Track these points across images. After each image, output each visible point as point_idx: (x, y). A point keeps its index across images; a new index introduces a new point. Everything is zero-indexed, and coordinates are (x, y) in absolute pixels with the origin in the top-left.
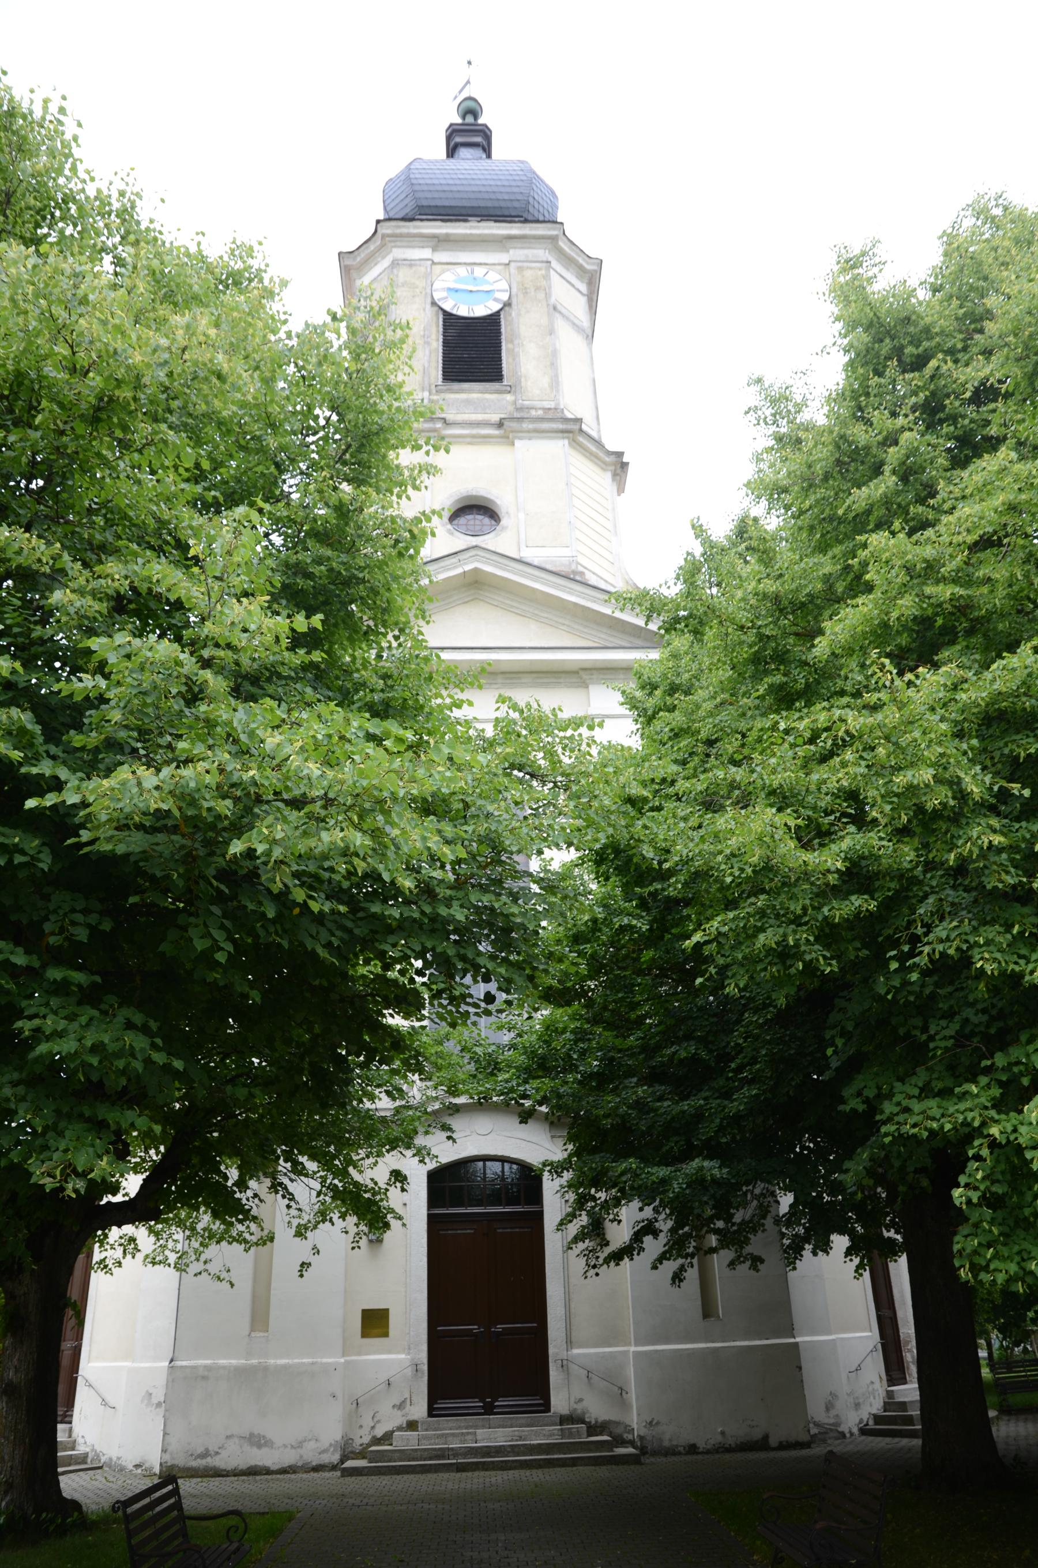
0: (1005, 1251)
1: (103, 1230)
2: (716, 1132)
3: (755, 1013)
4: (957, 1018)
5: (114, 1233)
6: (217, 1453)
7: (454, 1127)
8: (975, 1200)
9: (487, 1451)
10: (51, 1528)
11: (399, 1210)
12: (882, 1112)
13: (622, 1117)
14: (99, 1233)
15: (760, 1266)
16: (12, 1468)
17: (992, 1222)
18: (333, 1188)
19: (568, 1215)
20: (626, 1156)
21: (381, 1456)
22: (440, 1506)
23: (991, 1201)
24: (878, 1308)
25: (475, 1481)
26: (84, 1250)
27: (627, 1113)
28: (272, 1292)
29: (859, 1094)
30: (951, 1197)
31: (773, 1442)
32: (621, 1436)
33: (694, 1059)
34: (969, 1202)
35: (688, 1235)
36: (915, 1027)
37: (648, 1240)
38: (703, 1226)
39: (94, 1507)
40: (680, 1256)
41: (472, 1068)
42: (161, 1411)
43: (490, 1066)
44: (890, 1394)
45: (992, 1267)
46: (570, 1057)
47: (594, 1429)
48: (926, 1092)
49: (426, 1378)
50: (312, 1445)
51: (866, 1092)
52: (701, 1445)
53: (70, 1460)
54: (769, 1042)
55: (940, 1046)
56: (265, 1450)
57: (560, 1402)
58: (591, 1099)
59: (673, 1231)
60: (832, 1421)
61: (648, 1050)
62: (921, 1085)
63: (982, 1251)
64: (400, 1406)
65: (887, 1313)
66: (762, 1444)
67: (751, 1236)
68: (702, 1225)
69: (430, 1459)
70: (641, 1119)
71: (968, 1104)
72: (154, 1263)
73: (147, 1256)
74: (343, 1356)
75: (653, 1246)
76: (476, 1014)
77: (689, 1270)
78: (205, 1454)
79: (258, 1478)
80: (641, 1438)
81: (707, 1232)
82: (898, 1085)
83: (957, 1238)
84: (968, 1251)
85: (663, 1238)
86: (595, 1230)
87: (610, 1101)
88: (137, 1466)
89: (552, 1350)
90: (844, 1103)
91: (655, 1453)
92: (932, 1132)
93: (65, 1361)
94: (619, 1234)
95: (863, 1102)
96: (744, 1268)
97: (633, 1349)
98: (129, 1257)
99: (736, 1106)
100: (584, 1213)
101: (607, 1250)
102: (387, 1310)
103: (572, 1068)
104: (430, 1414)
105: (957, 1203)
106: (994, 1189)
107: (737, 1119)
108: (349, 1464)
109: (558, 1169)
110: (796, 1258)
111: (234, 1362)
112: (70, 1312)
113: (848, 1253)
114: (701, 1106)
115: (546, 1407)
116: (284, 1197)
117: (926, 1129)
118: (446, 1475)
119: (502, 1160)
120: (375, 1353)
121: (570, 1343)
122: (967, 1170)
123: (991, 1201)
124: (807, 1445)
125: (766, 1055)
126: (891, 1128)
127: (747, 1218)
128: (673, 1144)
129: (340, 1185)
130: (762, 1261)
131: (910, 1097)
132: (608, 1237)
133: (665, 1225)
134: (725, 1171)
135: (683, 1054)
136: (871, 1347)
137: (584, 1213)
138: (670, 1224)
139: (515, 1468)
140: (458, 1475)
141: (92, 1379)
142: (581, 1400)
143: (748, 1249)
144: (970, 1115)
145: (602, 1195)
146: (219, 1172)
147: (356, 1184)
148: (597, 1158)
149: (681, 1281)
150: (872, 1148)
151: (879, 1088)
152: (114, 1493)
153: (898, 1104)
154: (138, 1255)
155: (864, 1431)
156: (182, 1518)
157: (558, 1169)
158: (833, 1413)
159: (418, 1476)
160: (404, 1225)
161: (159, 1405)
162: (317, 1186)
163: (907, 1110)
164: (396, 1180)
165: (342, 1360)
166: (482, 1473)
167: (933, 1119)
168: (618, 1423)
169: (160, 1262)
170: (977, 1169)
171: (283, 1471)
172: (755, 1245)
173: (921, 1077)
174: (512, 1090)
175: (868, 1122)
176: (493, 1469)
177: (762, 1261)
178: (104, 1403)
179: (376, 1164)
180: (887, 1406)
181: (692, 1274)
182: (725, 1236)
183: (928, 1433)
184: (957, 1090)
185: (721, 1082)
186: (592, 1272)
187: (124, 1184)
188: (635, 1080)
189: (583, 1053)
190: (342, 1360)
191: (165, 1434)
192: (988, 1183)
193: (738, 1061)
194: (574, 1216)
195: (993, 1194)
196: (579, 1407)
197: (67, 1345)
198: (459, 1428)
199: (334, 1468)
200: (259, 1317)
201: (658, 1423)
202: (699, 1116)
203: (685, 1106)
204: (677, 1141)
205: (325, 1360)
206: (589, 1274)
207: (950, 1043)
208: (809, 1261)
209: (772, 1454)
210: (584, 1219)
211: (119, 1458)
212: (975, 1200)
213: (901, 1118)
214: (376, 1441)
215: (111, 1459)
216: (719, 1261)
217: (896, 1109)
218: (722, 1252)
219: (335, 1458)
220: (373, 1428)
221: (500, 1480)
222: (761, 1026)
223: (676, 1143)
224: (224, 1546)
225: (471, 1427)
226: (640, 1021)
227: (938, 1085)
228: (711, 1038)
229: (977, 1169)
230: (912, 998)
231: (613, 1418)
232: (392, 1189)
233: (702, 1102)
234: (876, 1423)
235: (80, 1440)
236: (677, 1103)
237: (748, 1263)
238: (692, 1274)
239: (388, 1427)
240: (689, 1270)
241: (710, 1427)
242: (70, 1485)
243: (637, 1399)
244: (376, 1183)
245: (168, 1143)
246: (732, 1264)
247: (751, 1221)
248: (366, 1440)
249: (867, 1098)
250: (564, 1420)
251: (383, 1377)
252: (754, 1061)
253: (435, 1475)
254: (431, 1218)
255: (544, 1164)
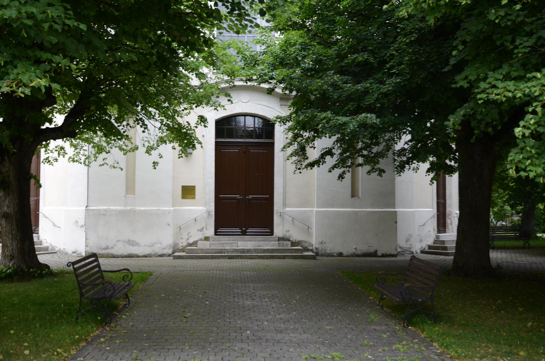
0: (537, 162)
1: (46, 141)
2: (375, 101)
3: (404, 37)
4: (535, 36)
5: (53, 144)
6: (112, 248)
7: (232, 95)
8: (527, 134)
9: (243, 251)
10: (36, 275)
11: (201, 139)
12: (478, 87)
13: (324, 90)
14: (44, 143)
15: (383, 174)
16: (12, 250)
17: (532, 147)
18: (167, 125)
19: (288, 143)
20: (325, 111)
21: (192, 251)
22: (222, 272)
23: (536, 136)
24: (438, 198)
25: (237, 263)
26: (36, 152)
27: (327, 89)
28: (136, 176)
29: (466, 78)
30: (513, 131)
31: (379, 253)
32: (307, 247)
33: (366, 63)
34: (524, 135)
35: (348, 157)
36: (506, 41)
37: (328, 158)
38: (356, 153)
39: (56, 268)
40: (343, 167)
41: (242, 64)
42: (83, 229)
43: (252, 62)
44: (437, 237)
45: (528, 169)
46: (297, 59)
47: (293, 244)
48: (507, 77)
49: (214, 218)
50: (159, 245)
51: (470, 78)
52: (345, 253)
53: (40, 249)
54: (410, 53)
55: (520, 52)
56: (136, 247)
57: (278, 231)
58: (308, 81)
59: (341, 154)
60: (408, 246)
61: (341, 57)
62: (504, 73)
63: (524, 161)
64: (201, 230)
65: (441, 201)
66: (374, 254)
67: (380, 160)
68: (358, 151)
69: (216, 253)
70: (334, 93)
71: (534, 83)
72: (74, 161)
73: (70, 158)
74: (173, 207)
75: (330, 161)
76: (251, 26)
77: (347, 173)
78: (107, 248)
79: (133, 259)
80: (317, 249)
81: (358, 156)
82: (490, 74)
83: (511, 154)
84: (516, 161)
85: (336, 158)
86: (301, 152)
87: (318, 82)
88: (74, 252)
89: (276, 208)
90: (456, 83)
91: (322, 255)
92: (508, 99)
93: (32, 207)
94: (313, 154)
95: (468, 83)
96: (374, 175)
97: (315, 209)
98: (61, 157)
99: (385, 89)
100: (296, 143)
101: (307, 162)
102: (194, 186)
103: (298, 65)
104: (216, 234)
105: (517, 135)
106: (538, 129)
107: (386, 95)
108: (176, 254)
109: (283, 120)
110: (401, 171)
111: (118, 208)
112: (32, 181)
113: (428, 171)
114: (368, 88)
115: (272, 233)
116: (141, 127)
117: (505, 96)
118: (223, 260)
119: (254, 116)
120: (188, 206)
121: (285, 205)
122: (525, 119)
123: (536, 136)
124: (395, 256)
125: (408, 60)
126: (484, 96)
127: (380, 150)
128: (351, 106)
129: (171, 124)
130: (384, 172)
131: (497, 80)
132: (308, 155)
133: (337, 152)
134: (378, 120)
135: (360, 59)
136: (432, 215)
137: (296, 143)
138: (339, 151)
139: (256, 258)
140: (229, 260)
141: (47, 215)
142: (289, 231)
143: (378, 166)
144: (533, 89)
145: (306, 134)
146: (106, 114)
147: (179, 124)
148: (309, 111)
149: (343, 178)
150: (466, 108)
151: (479, 76)
152: (64, 263)
153: (490, 83)
154: (66, 156)
155: (423, 252)
156: (100, 271)
157: (283, 120)
158: (409, 243)
159: (210, 260)
160: (202, 147)
161: (82, 226)
162: (158, 125)
163: (494, 87)
164: (201, 121)
165: (172, 209)
166: (241, 260)
167: (509, 91)
168: (306, 242)
169: (77, 161)
170: (531, 119)
171: (145, 256)
172: (382, 163)
173: (505, 69)
174: (265, 75)
175: (465, 95)
176: (246, 258)
177: (384, 172)
178: (54, 225)
179: (189, 113)
180: (435, 242)
181: (348, 176)
182: (367, 159)
183: (456, 255)
184: (528, 75)
185: (380, 75)
186: (298, 171)
187: (54, 120)
188: (332, 72)
189: (304, 57)
190: (172, 209)
191: (86, 239)
192: (536, 126)
193: (391, 64)
194: (291, 144)
195: (537, 131)
196: (288, 234)
197: (32, 199)
198: (230, 240)
199: (169, 255)
200: (130, 187)
201: (325, 243)
202: (366, 92)
203: (359, 87)
204: (356, 104)
205: (164, 208)
206: (296, 172)
207: (527, 50)
208: (408, 174)
209: (378, 259)
210: (295, 146)
211: (64, 249)
212: (527, 134)
213: (490, 91)
214: (190, 245)
215: (60, 249)
216: (362, 171)
217: (488, 86)
218: (364, 166)
219: (170, 251)
220: (188, 239)
221: (249, 263)
222: (407, 44)
223: (353, 105)
224: (122, 283)
225: (235, 240)
226: (336, 43)
227: (514, 74)
228: (376, 51)
229: (531, 119)
230: (509, 23)
231: (304, 240)
232: (199, 126)
233: (368, 85)
234: (429, 249)
235: (44, 241)
236: (354, 85)
237: (377, 173)
238: (348, 176)
239: (195, 239)
240: (347, 173)
241: (349, 246)
242: (42, 259)
243: (316, 232)
244: (189, 124)
245: (78, 98)
246: (369, 173)
247: (381, 152)
248: (185, 244)
249: (470, 80)
250: (280, 239)
251: (193, 217)
252: (400, 64)
253: (218, 260)
254: (217, 144)
255: (277, 118)
